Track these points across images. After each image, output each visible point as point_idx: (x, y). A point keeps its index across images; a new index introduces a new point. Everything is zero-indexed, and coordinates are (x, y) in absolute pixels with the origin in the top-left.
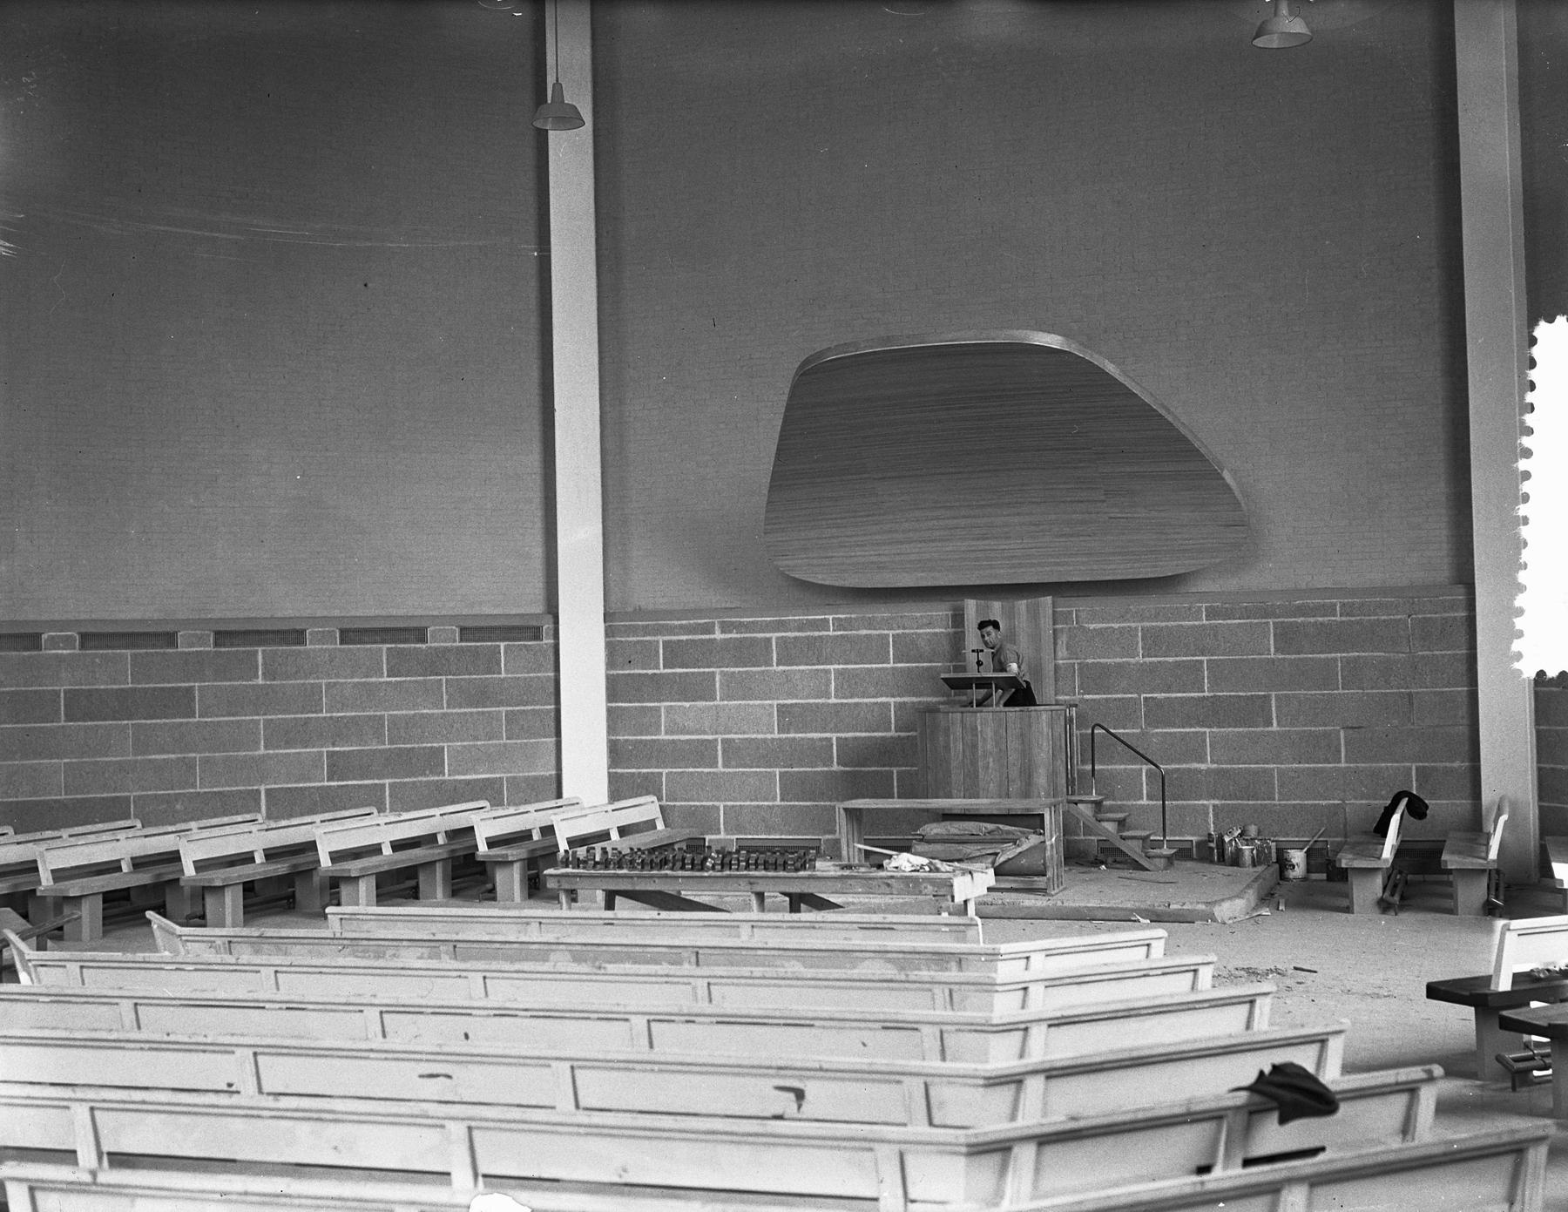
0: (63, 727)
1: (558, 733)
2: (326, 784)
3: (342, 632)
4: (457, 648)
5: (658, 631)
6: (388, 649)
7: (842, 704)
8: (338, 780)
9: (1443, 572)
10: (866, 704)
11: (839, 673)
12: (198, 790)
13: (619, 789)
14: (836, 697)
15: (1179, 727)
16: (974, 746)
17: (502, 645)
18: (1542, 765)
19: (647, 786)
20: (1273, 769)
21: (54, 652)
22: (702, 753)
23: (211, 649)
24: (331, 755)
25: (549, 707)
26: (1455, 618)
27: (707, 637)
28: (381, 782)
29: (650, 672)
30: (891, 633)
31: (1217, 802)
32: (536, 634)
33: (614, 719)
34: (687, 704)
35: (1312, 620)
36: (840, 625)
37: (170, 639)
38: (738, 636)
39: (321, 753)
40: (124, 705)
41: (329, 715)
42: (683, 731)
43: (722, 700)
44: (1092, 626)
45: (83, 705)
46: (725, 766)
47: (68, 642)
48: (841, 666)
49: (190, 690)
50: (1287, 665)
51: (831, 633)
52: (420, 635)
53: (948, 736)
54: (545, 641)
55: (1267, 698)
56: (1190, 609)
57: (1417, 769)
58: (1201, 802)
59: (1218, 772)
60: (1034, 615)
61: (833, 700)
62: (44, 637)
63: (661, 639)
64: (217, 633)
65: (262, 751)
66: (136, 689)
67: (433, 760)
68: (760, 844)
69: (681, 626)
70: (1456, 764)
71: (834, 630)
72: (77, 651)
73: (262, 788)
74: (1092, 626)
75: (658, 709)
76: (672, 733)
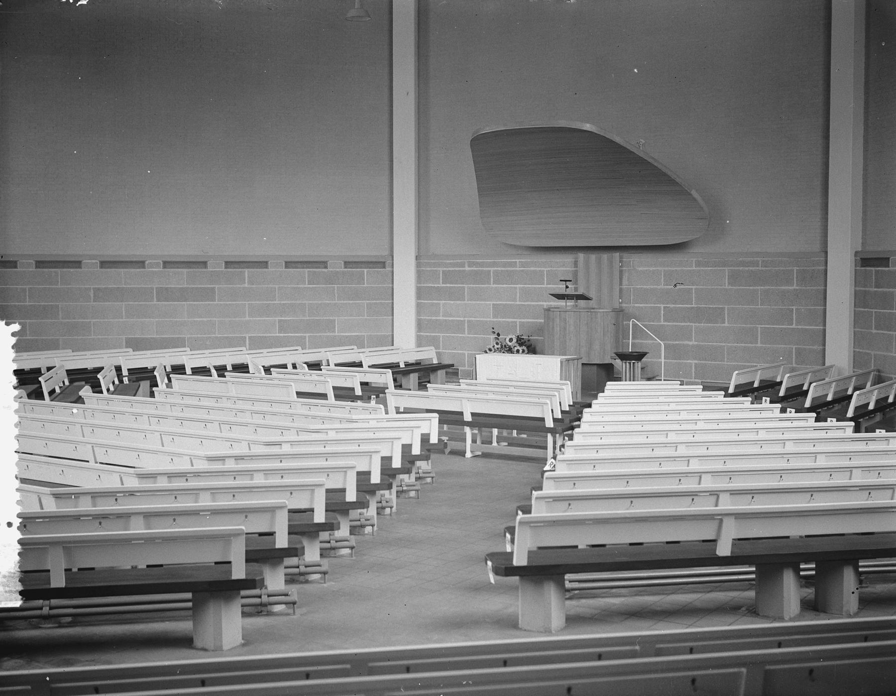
0: (155, 304)
1: (393, 315)
2: (278, 335)
3: (286, 262)
4: (343, 271)
5: (439, 265)
6: (308, 271)
7: (522, 305)
8: (284, 333)
9: (817, 247)
10: (533, 305)
11: (521, 289)
12: (217, 335)
13: (420, 342)
14: (520, 301)
15: (680, 322)
16: (565, 329)
17: (365, 270)
18: (855, 350)
19: (434, 342)
20: (724, 346)
21: (151, 269)
22: (458, 327)
23: (223, 269)
24: (280, 321)
25: (822, 259)
26: (819, 270)
27: (461, 269)
28: (305, 335)
29: (436, 285)
30: (545, 269)
31: (696, 362)
32: (383, 265)
33: (419, 308)
34: (452, 302)
35: (747, 269)
36: (523, 265)
37: (204, 264)
38: (476, 269)
39: (275, 320)
40: (183, 295)
41: (279, 302)
42: (451, 316)
43: (468, 301)
44: (640, 269)
45: (165, 294)
46: (468, 334)
47: (157, 265)
48: (522, 286)
49: (213, 289)
50: (869, 285)
51: (518, 269)
52: (324, 264)
53: (554, 322)
54: (387, 269)
55: (723, 309)
56: (687, 261)
57: (796, 348)
58: (688, 361)
59: (697, 346)
60: (611, 262)
61: (518, 303)
62: (147, 262)
63: (441, 269)
64: (226, 263)
65: (247, 318)
66: (188, 287)
67: (330, 325)
68: (713, 385)
69: (450, 263)
70: (815, 347)
71: (519, 267)
72: (161, 269)
73: (247, 336)
74: (640, 269)
75: (439, 304)
76: (446, 316)
